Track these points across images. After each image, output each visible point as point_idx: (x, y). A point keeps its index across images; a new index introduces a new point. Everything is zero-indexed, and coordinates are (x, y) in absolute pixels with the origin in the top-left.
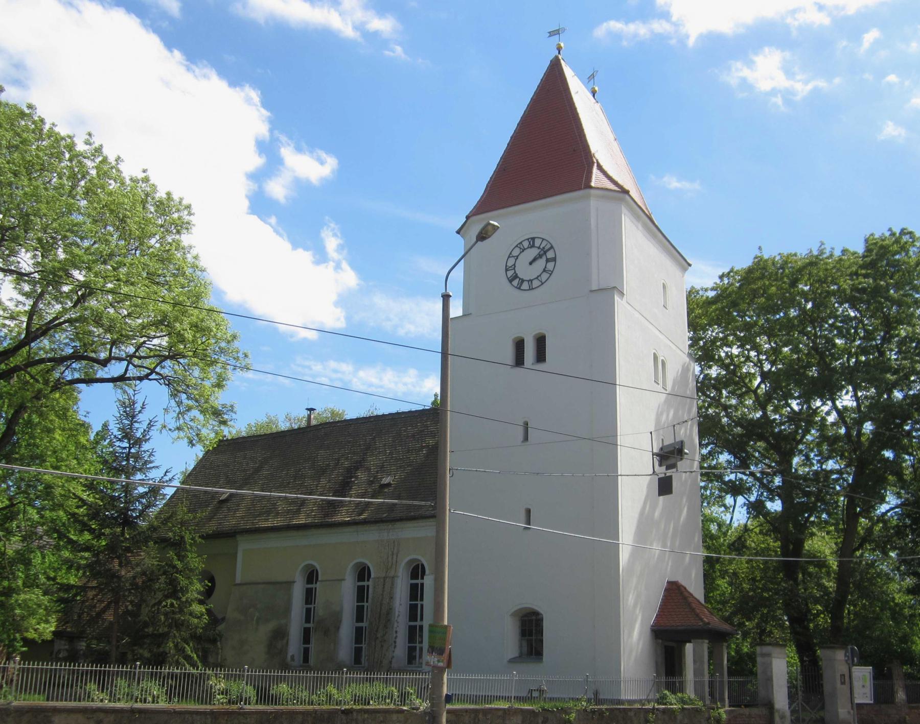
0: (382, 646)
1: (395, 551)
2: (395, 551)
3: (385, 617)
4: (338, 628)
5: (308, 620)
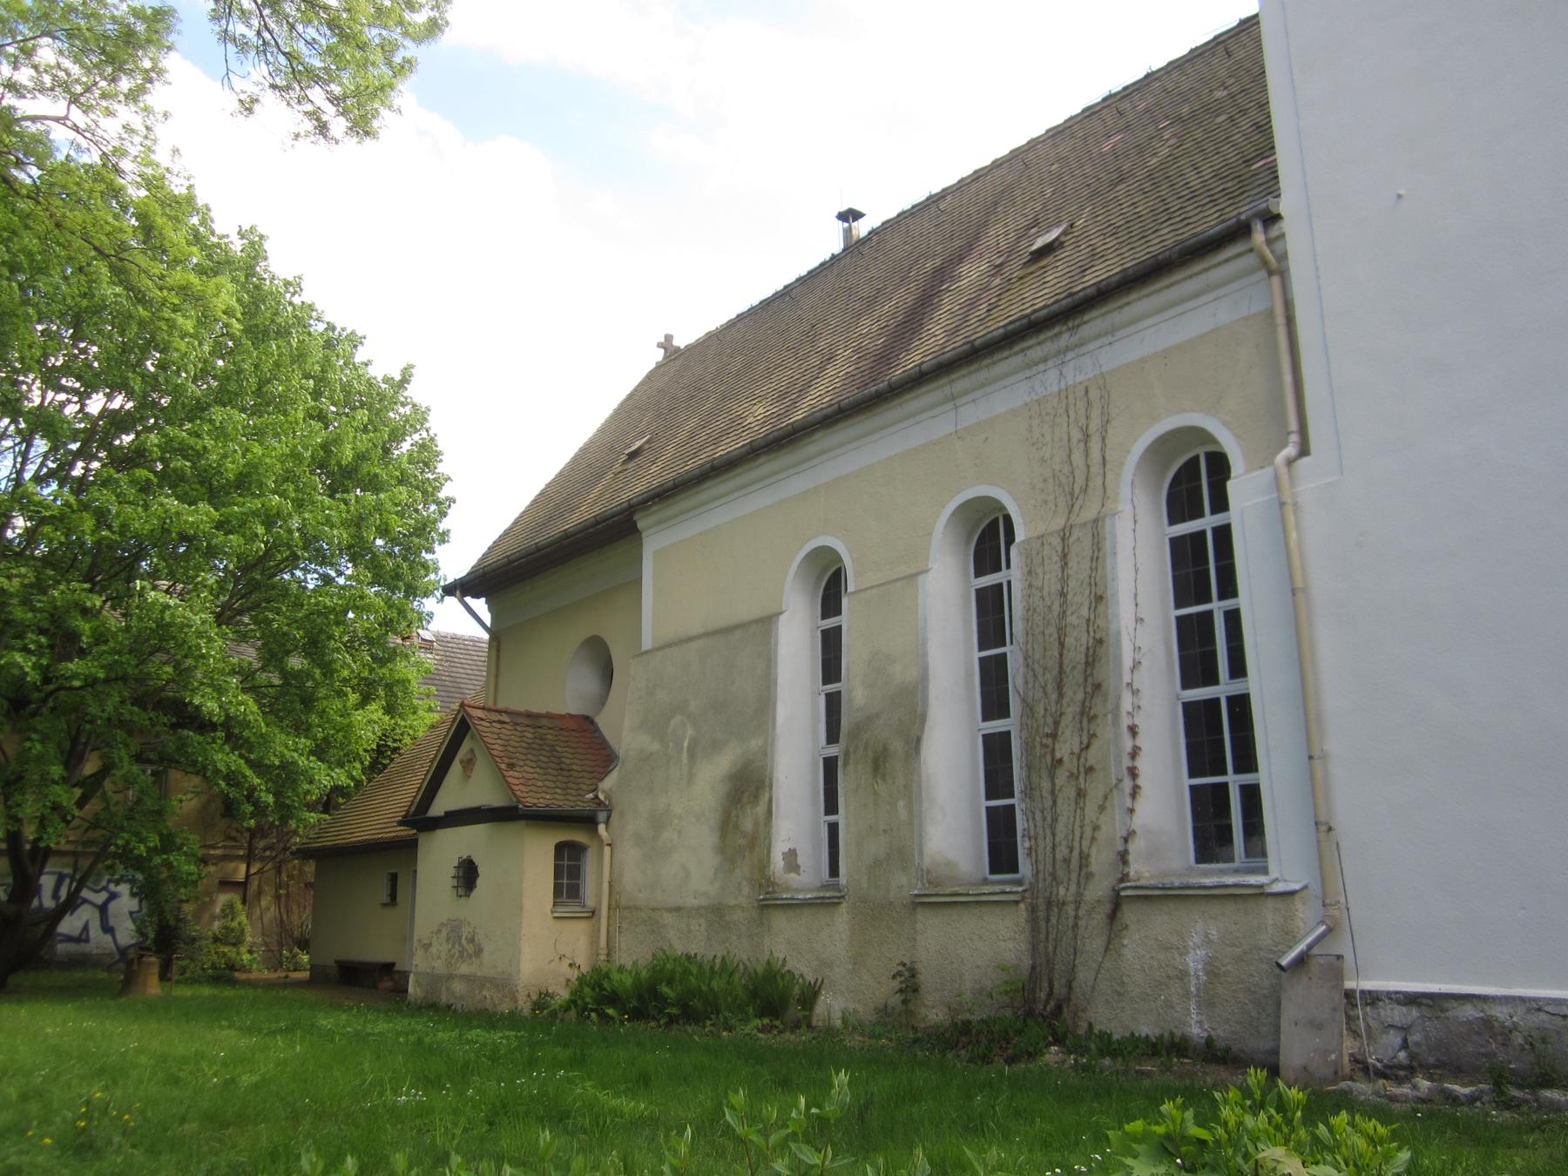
0: (1081, 794)
1: (1095, 425)
2: (1095, 425)
3: (1088, 673)
4: (914, 745)
5: (833, 736)
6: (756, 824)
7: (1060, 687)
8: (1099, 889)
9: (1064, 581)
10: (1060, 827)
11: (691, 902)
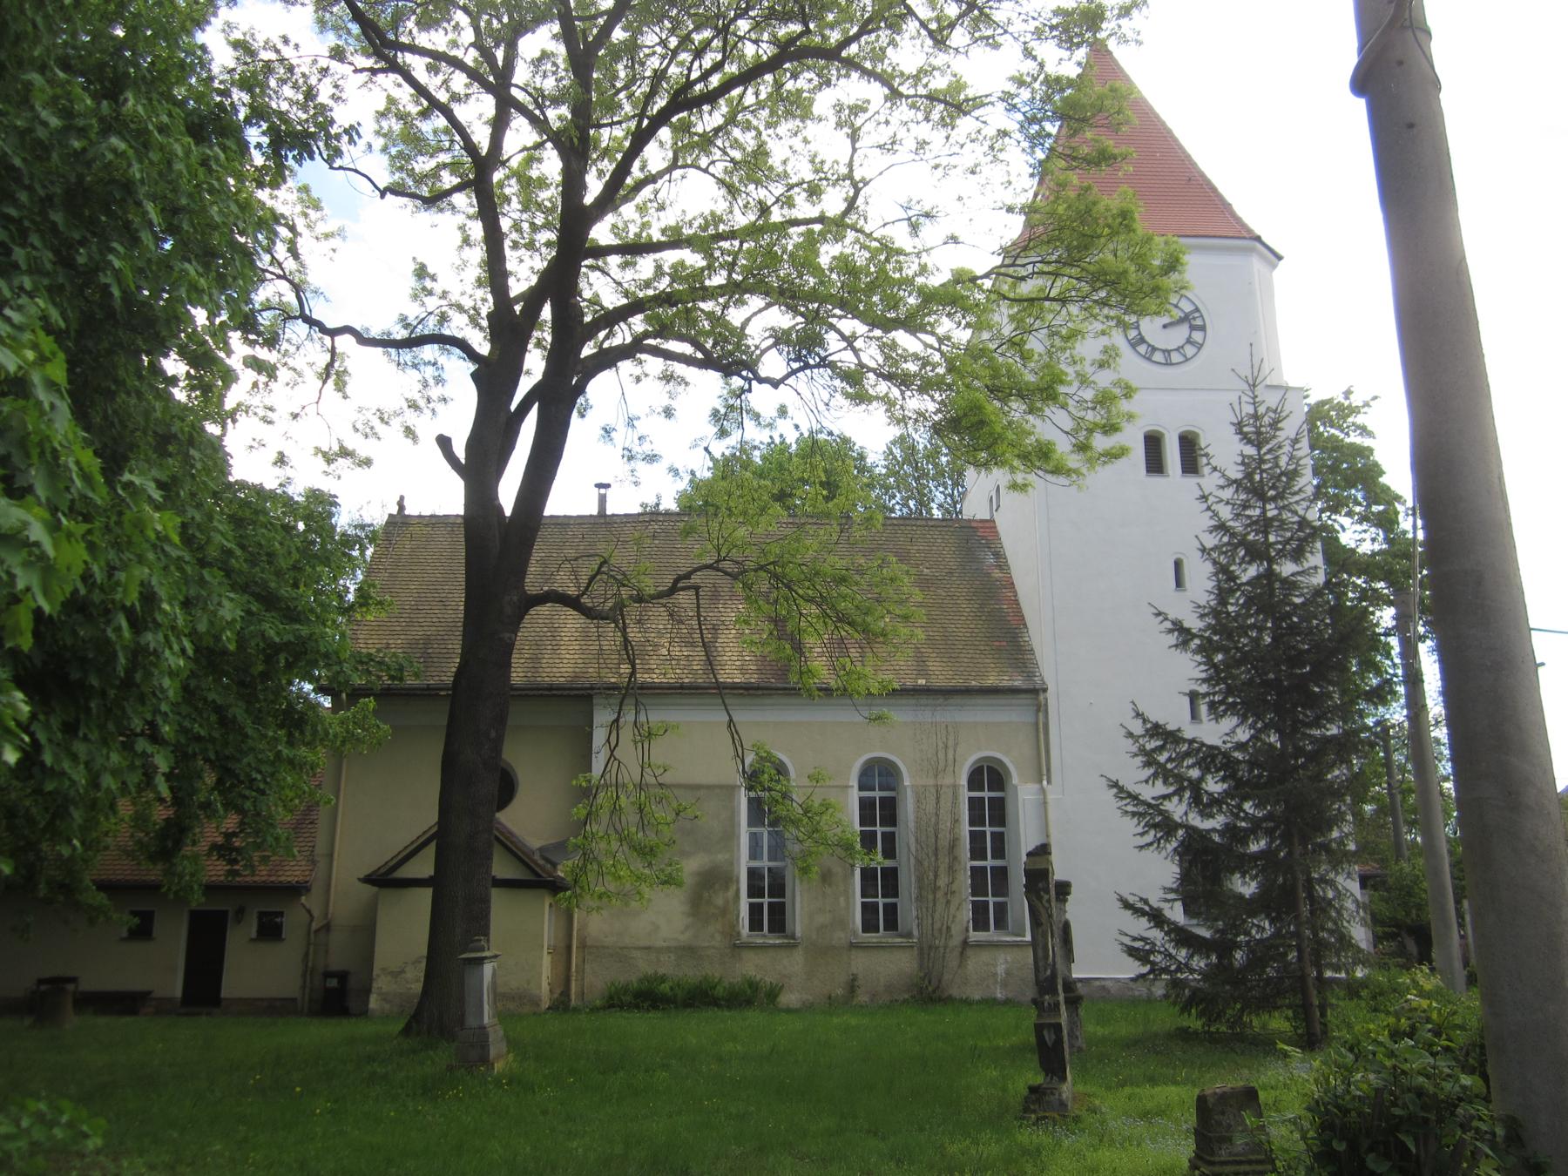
0: (948, 902)
1: (950, 743)
6: (727, 902)
7: (936, 855)
8: (956, 941)
9: (937, 808)
10: (937, 916)
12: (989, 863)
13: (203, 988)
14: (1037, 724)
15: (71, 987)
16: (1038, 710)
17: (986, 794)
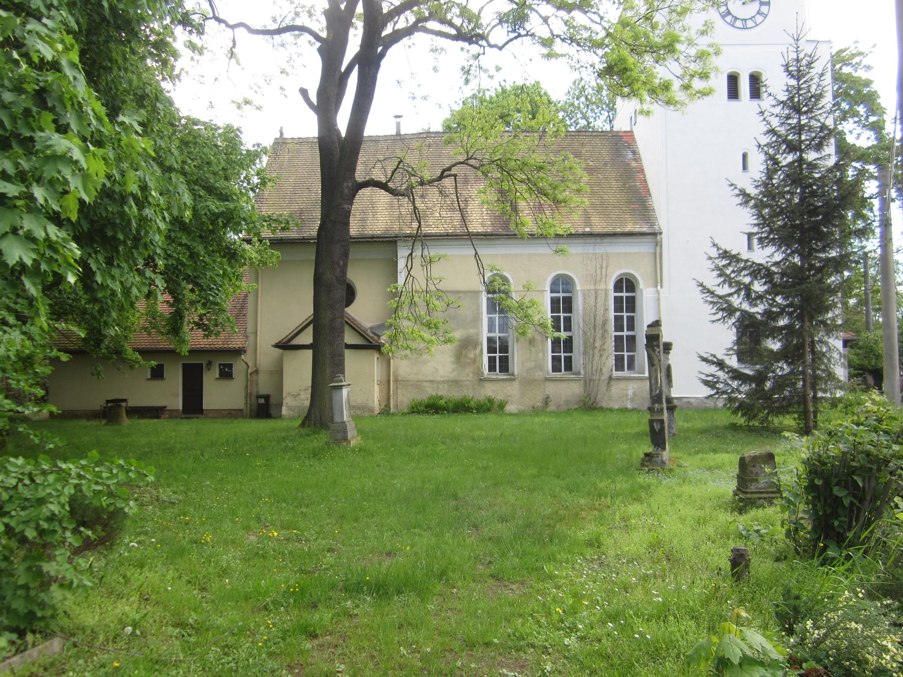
0: (601, 355)
1: (604, 265)
8: (605, 377)
10: (595, 363)
11: (439, 379)
12: (625, 333)
13: (193, 404)
14: (655, 253)
15: (124, 404)
16: (656, 245)
17: (624, 294)
